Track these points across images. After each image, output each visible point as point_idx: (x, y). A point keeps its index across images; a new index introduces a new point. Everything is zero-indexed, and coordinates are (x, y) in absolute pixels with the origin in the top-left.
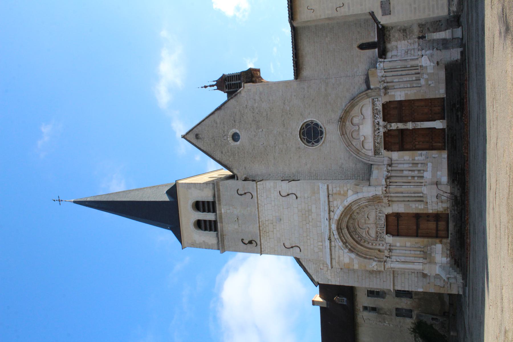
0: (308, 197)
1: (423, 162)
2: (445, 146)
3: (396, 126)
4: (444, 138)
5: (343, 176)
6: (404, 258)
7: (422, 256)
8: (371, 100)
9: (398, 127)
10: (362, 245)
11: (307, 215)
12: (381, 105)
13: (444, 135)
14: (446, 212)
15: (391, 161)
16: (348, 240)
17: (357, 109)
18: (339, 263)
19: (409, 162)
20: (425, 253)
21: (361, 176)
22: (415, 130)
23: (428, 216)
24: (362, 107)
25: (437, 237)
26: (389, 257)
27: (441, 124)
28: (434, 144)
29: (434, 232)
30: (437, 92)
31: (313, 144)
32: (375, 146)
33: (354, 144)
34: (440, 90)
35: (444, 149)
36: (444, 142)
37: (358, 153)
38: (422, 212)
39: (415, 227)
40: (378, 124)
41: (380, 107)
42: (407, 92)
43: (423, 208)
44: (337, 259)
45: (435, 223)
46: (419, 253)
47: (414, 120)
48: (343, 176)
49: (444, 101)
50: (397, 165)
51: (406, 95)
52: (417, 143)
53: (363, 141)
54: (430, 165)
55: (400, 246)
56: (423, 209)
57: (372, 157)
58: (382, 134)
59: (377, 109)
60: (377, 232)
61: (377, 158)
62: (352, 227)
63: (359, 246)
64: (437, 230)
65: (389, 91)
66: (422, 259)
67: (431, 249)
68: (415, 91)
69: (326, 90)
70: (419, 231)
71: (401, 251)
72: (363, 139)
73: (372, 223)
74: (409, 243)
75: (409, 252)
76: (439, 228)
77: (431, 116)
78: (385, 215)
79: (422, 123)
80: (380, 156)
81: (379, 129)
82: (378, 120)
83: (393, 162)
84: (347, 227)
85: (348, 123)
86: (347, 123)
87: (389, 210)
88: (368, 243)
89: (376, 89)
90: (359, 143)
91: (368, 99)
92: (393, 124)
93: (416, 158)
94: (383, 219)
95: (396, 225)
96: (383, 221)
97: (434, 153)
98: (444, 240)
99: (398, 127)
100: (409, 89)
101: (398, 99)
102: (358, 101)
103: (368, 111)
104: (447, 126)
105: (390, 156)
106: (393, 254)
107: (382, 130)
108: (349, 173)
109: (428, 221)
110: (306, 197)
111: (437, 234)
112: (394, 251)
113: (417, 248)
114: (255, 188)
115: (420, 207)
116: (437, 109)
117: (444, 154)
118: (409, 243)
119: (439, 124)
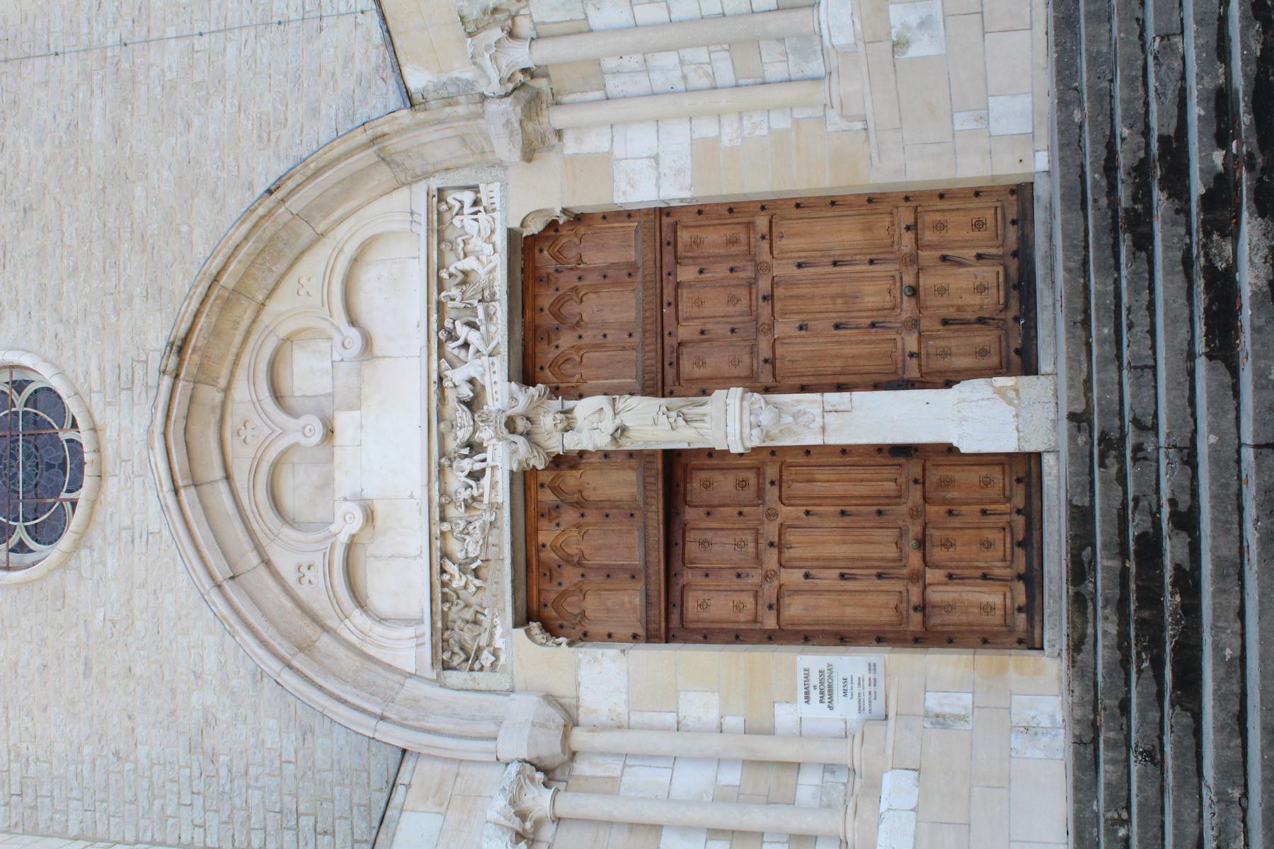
1: (838, 752)
2: (1032, 608)
3: (609, 425)
4: (1031, 542)
5: (213, 820)
8: (421, 207)
9: (622, 430)
12: (500, 240)
13: (1032, 514)
15: (571, 723)
17: (312, 281)
19: (715, 744)
21: (342, 828)
22: (773, 465)
24: (355, 261)
27: (1005, 412)
28: (938, 595)
30: (963, 122)
31: (21, 547)
32: (442, 594)
33: (285, 563)
34: (997, 105)
35: (1031, 642)
36: (1032, 579)
37: (305, 648)
40: (471, 405)
41: (489, 263)
42: (707, 129)
47: (769, 379)
48: (213, 820)
49: (1024, 220)
50: (612, 768)
51: (705, 152)
52: (792, 577)
53: (351, 546)
54: (897, 789)
57: (412, 686)
58: (497, 489)
59: (466, 278)
61: (453, 697)
65: (558, 118)
68: (780, 122)
69: (117, 135)
72: (356, 524)
77: (911, 343)
79: (833, 398)
80: (484, 679)
81: (473, 447)
82: (472, 368)
83: (579, 738)
85: (247, 394)
86: (241, 391)
89: (450, 101)
90: (318, 559)
91: (401, 196)
92: (584, 408)
93: (785, 716)
97: (941, 679)
99: (622, 430)
100: (723, 99)
101: (640, 191)
102: (322, 207)
103: (398, 299)
104: (1068, 140)
105: (563, 689)
107: (502, 457)
108: (255, 797)
114: (736, 526)
116: (971, 286)
117: (1038, 692)
119: (981, 417)
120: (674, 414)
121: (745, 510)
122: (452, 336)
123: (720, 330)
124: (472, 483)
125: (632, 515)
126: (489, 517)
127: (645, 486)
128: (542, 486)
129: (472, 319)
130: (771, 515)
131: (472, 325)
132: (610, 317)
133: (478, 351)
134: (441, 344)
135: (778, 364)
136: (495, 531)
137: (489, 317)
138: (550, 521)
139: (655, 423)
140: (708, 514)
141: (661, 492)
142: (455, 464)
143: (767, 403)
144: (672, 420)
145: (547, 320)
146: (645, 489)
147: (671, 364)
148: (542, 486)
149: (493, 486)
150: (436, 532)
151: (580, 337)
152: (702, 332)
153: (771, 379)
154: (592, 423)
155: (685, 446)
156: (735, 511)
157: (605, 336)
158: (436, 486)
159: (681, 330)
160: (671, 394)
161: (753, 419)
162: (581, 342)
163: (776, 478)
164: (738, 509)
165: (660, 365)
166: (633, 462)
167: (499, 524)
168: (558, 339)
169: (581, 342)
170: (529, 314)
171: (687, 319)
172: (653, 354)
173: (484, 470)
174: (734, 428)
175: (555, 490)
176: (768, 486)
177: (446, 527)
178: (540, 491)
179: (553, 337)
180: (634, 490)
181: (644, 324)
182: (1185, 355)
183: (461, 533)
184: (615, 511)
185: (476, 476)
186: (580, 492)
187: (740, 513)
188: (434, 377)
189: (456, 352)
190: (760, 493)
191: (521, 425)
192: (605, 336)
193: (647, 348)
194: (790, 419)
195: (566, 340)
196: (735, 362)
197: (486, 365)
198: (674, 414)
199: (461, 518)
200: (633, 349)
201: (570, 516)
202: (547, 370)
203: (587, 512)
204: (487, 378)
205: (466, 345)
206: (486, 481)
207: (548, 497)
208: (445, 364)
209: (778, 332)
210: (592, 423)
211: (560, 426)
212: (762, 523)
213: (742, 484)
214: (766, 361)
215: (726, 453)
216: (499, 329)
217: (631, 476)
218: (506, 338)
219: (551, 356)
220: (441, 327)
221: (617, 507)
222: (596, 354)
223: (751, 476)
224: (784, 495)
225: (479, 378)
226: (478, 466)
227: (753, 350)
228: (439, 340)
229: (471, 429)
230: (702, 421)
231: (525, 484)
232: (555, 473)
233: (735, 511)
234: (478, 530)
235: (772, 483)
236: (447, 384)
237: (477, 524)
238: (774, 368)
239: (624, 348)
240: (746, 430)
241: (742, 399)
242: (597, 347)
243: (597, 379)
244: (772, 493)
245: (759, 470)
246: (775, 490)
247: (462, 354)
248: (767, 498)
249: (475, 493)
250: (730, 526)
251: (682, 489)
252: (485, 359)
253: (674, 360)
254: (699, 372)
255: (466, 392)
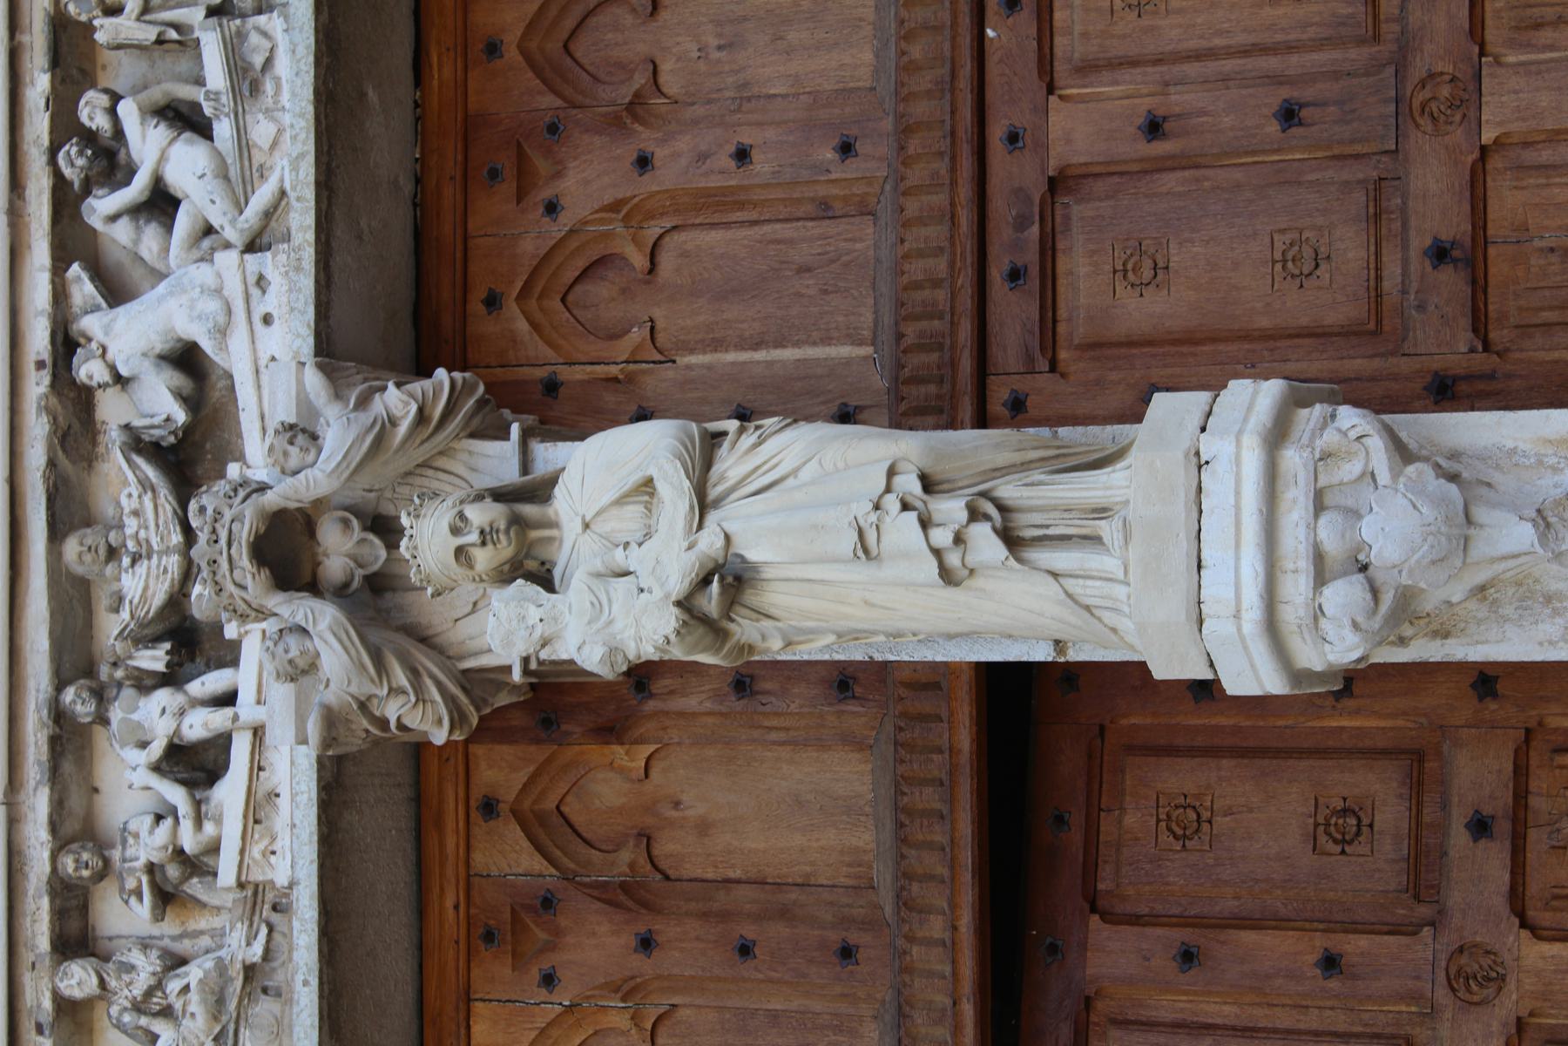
3: (670, 560)
9: (730, 579)
40: (186, 459)
92: (602, 472)
99: (730, 579)
114: (1311, 1021)
120: (951, 509)
121: (1354, 946)
122: (110, 162)
123: (1226, 112)
124: (177, 795)
125: (847, 953)
126: (242, 947)
127: (903, 819)
128: (489, 807)
129: (186, 92)
130: (1473, 976)
131: (186, 119)
132: (771, 71)
133: (209, 230)
134: (66, 202)
135: (1499, 266)
136: (264, 1008)
137: (247, 80)
138: (519, 960)
139: (864, 550)
140: (1188, 957)
141: (967, 857)
142: (116, 714)
143: (1403, 453)
144: (942, 537)
145: (519, 94)
146: (902, 840)
147: (1015, 275)
148: (489, 807)
149: (257, 810)
150: (39, 998)
151: (644, 162)
152: (1154, 128)
153: (1464, 339)
154: (613, 545)
155: (1041, 653)
156: (1302, 949)
157: (742, 155)
158: (38, 804)
159: (1060, 119)
160: (1018, 412)
161: (1329, 532)
162: (649, 184)
163: (1498, 801)
164: (1321, 942)
165: (966, 279)
166: (857, 717)
167: (278, 978)
168: (558, 175)
169: (649, 184)
170: (442, 69)
171: (1087, 68)
172: (935, 233)
173: (221, 744)
174: (1233, 578)
175: (546, 827)
176: (1459, 837)
177: (78, 979)
178: (480, 828)
179: (542, 165)
180: (864, 838)
181: (904, 97)
182: (750, 597)
183: (138, 1008)
184: (778, 931)
185: (194, 764)
186: (646, 838)
187: (1330, 963)
188: (39, 340)
189: (122, 232)
190: (1423, 872)
191: (338, 547)
192: (742, 155)
193: (912, 207)
194: (1521, 535)
195: (588, 180)
196: (1297, 263)
197: (234, 289)
198: (951, 509)
199: (145, 945)
200: (865, 210)
201: (595, 945)
202: (511, 308)
203: (666, 930)
204: (238, 341)
205: (161, 204)
206: (230, 793)
207: (510, 857)
208: (83, 288)
209: (1499, 114)
210: (613, 545)
211: (484, 559)
212: (1432, 1013)
213: (1343, 826)
214: (1440, 254)
215: (1206, 690)
216: (285, 133)
217: (851, 776)
218: (308, 170)
219: (530, 247)
220: (65, 126)
221: (785, 914)
222: (715, 236)
223: (1382, 791)
224: (1534, 887)
225: (207, 345)
226: (199, 725)
227: (1380, 206)
228: (60, 184)
229: (173, 562)
230: (1094, 540)
231: (418, 799)
232: (540, 753)
233: (1302, 949)
234: (195, 1003)
235: (1480, 827)
236: (89, 370)
237: (194, 973)
238: (1479, 286)
239: (825, 210)
240: (1296, 587)
241: (1278, 435)
242: (713, 206)
243: (717, 345)
244: (1478, 874)
245: (1419, 764)
246: (1493, 860)
247: (149, 240)
248: (1455, 898)
249: (189, 841)
250: (1284, 1019)
251: (1075, 837)
252: (228, 260)
253: (1031, 257)
254: (1140, 310)
255: (160, 403)
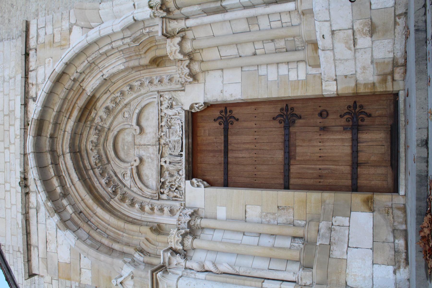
0: (10, 78)
6: (232, 259)
7: (296, 254)
10: (111, 211)
11: (7, 125)
14: (389, 87)
16: (72, 190)
18: (45, 259)
20: (307, 243)
23: (321, 108)
25: (355, 188)
26: (185, 254)
29: (346, 169)
38: (299, 93)
39: (280, 155)
43: (302, 77)
44: (42, 246)
45: (348, 136)
46: (287, 243)
51: (402, 121)
55: (229, 219)
56: (305, 83)
60: (161, 171)
62: (93, 155)
63: (99, 211)
64: (355, 164)
66: (295, 267)
67: (330, 230)
70: (294, 169)
71: (229, 236)
73: (147, 137)
74: (258, 209)
75: (253, 240)
76: (362, 157)
78: (183, 114)
84: (76, 153)
87: (195, 96)
88: (132, 204)
94: (178, 128)
95: (215, 145)
96: (177, 135)
98: (383, 199)
106: (197, 243)
109: (324, 129)
110: (7, 78)
111: (355, 176)
112: (207, 235)
113: (285, 224)
115: (293, 76)
118: (258, 209)
